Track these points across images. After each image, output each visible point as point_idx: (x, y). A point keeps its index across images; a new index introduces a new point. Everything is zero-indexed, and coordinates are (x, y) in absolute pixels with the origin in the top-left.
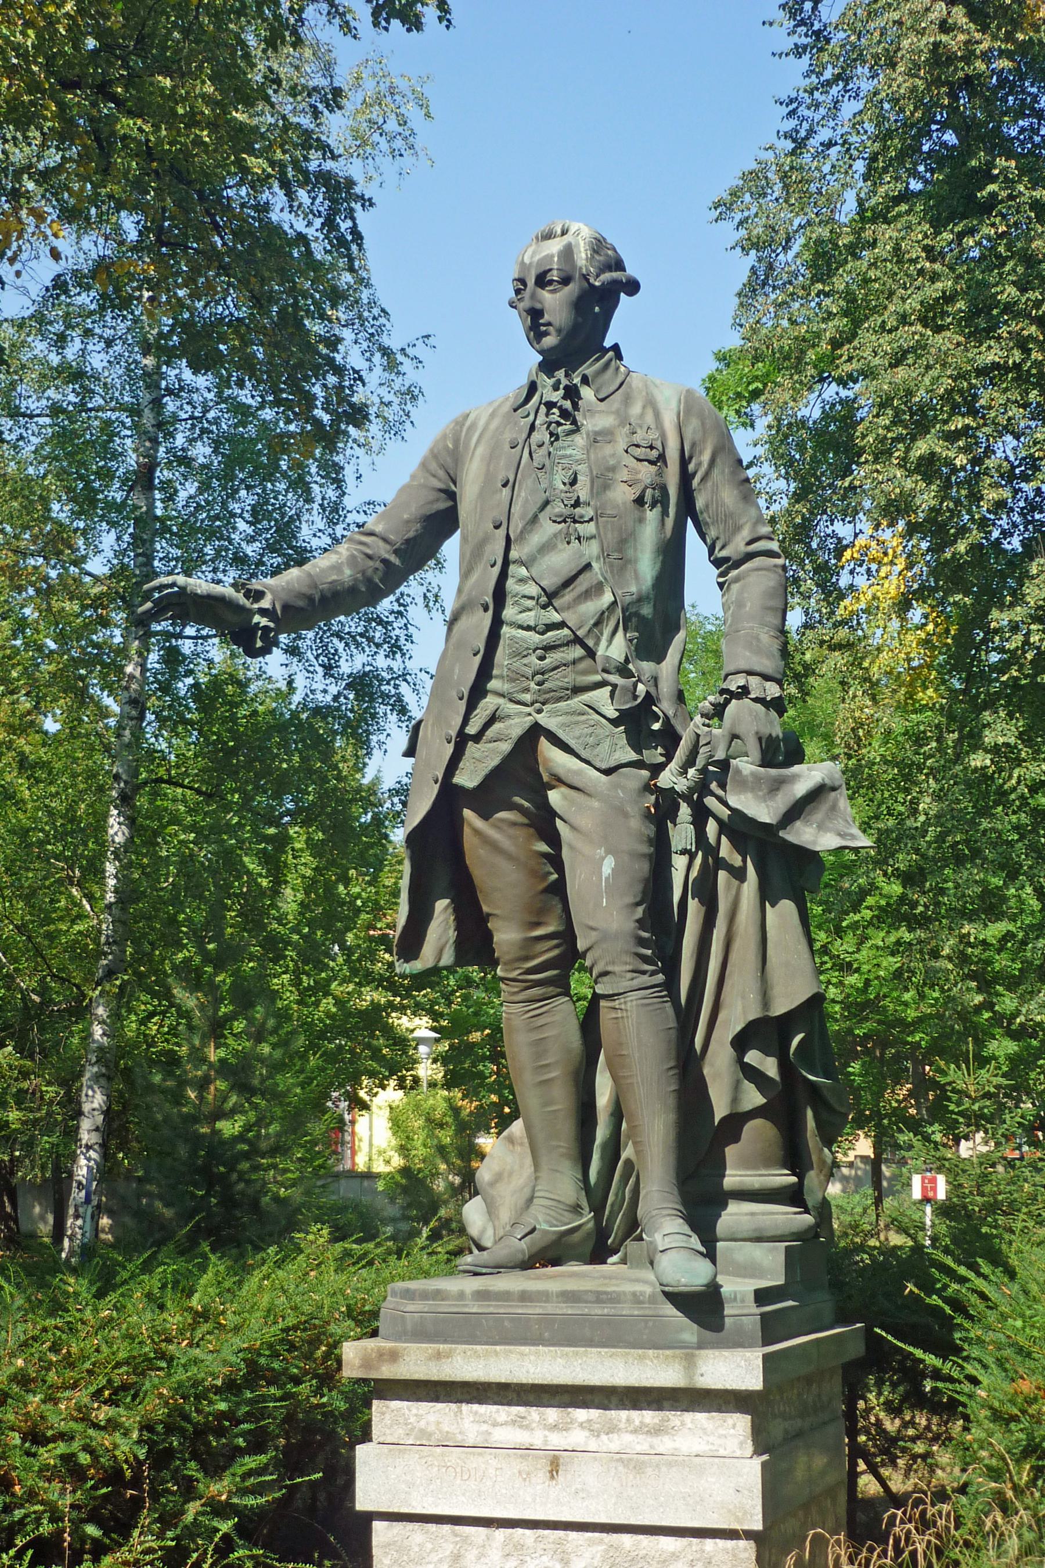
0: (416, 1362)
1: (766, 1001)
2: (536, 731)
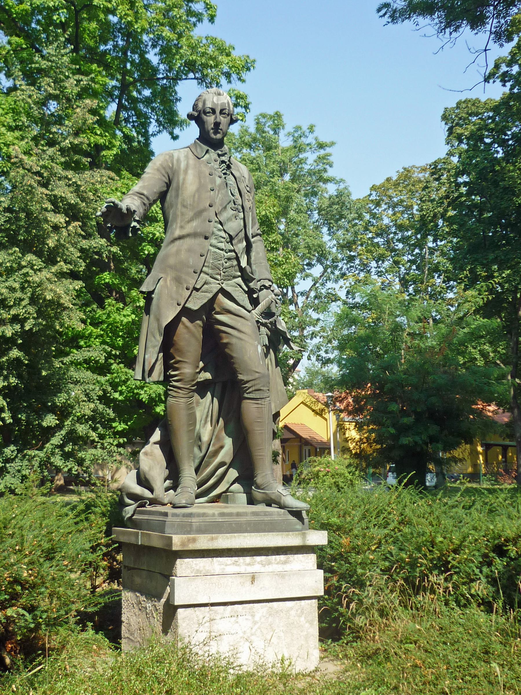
0: (203, 542)
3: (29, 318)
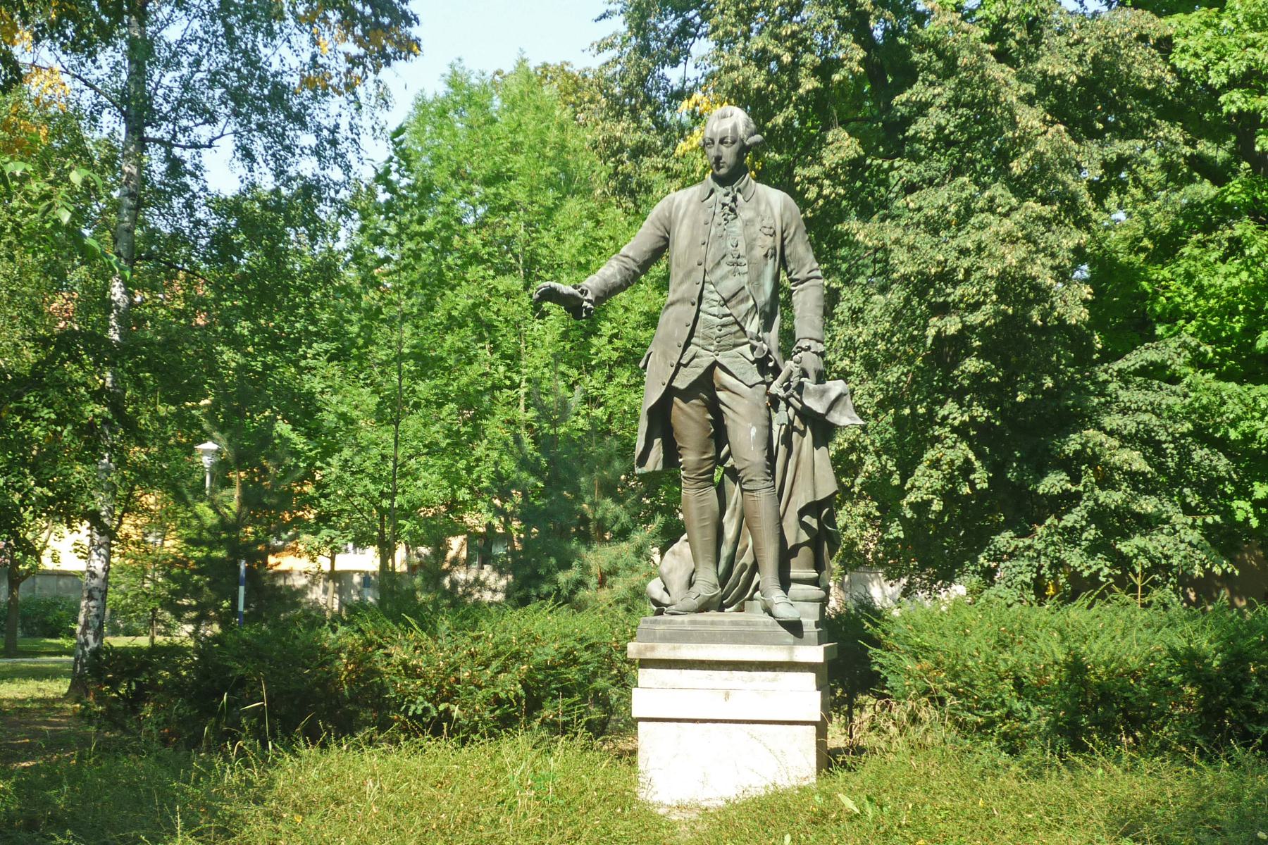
0: (664, 651)
1: (815, 496)
2: (715, 363)
3: (984, 303)
